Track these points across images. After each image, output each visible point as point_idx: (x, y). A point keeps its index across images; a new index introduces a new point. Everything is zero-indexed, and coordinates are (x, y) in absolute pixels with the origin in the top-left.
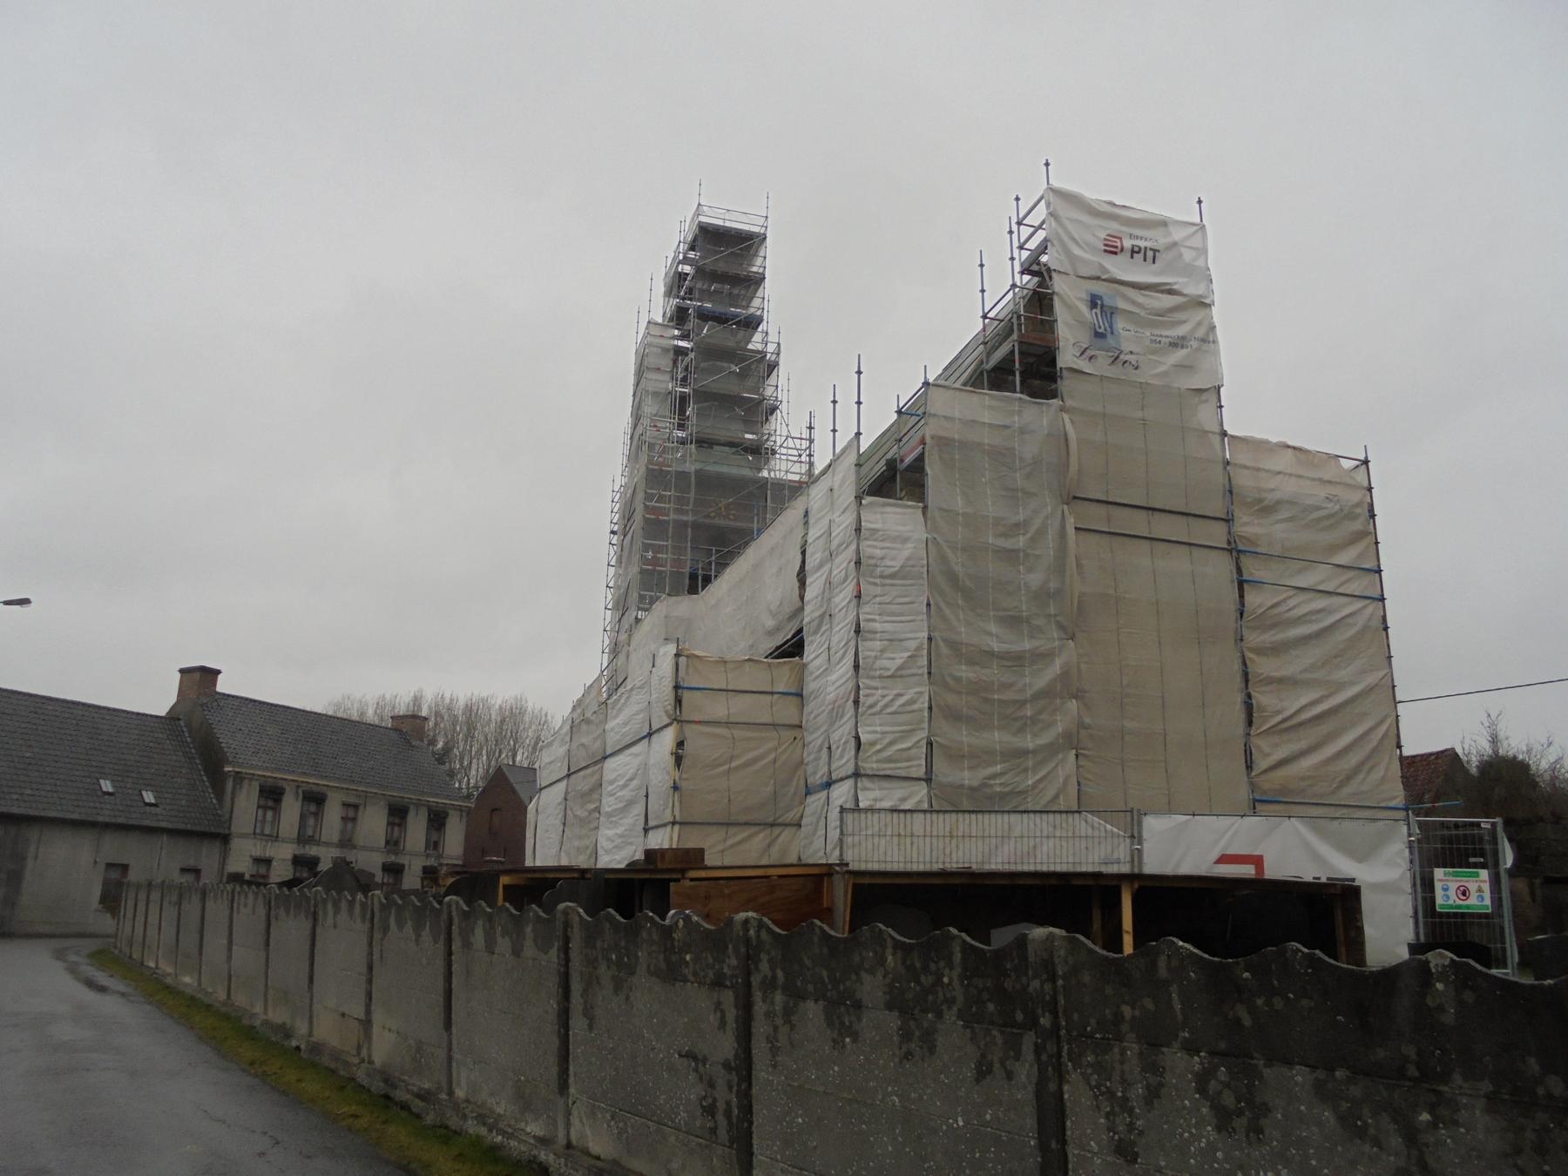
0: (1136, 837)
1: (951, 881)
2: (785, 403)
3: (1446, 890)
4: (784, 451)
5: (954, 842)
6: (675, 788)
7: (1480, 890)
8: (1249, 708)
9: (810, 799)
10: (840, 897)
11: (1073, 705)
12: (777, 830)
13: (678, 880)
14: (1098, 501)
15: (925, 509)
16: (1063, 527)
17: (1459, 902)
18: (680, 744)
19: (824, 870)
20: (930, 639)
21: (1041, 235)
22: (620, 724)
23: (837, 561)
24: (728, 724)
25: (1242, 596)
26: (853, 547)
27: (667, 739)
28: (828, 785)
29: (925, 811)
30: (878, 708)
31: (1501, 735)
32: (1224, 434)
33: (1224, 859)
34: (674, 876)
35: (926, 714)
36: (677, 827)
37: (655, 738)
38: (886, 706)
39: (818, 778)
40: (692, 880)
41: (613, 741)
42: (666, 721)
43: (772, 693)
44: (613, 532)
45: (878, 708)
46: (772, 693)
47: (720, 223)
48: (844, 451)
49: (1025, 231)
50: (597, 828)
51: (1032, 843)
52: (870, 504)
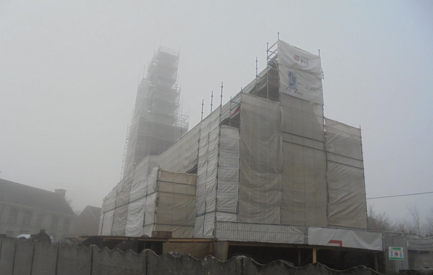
0: (306, 234)
1: (116, 239)
2: (181, 105)
3: (392, 253)
4: (180, 119)
5: (251, 233)
6: (156, 213)
7: (401, 253)
8: (328, 198)
9: (197, 218)
10: (223, 250)
11: (280, 193)
12: (186, 228)
13: (165, 242)
14: (288, 133)
15: (240, 130)
16: (279, 139)
17: (395, 257)
18: (158, 199)
19: (210, 240)
20: (240, 170)
21: (274, 55)
22: (134, 193)
23: (211, 145)
24: (173, 193)
25: (327, 164)
26: (218, 140)
27: (154, 196)
28: (205, 214)
29: (236, 223)
30: (223, 190)
31: (373, 211)
32: (324, 117)
33: (331, 242)
34: (164, 241)
35: (237, 193)
36: (155, 225)
37: (148, 197)
38: (226, 190)
39: (202, 211)
40: (170, 242)
41: (132, 197)
42: (153, 191)
43: (187, 185)
44: (127, 139)
45: (223, 190)
46: (187, 185)
47: (166, 52)
48: (215, 111)
49: (270, 53)
50: (125, 224)
51: (275, 234)
52: (223, 127)
